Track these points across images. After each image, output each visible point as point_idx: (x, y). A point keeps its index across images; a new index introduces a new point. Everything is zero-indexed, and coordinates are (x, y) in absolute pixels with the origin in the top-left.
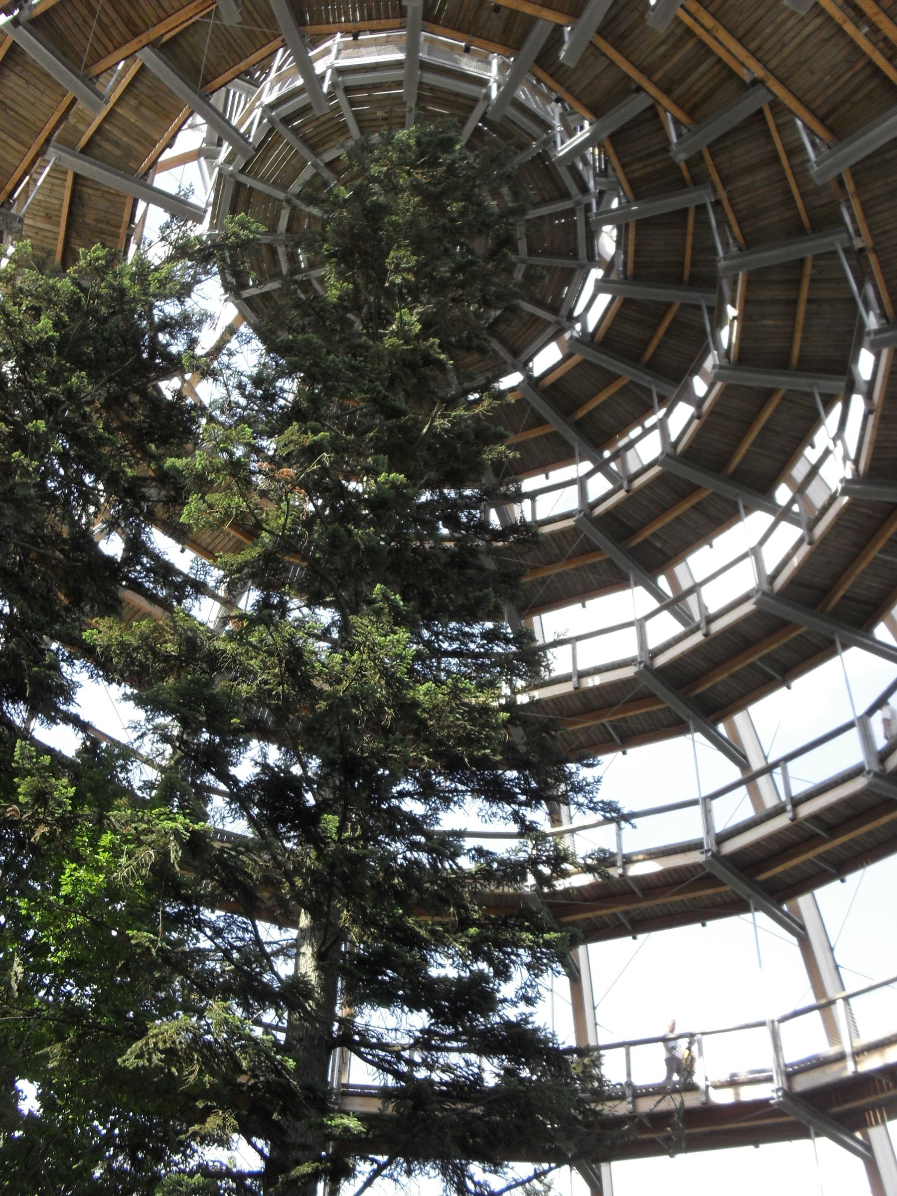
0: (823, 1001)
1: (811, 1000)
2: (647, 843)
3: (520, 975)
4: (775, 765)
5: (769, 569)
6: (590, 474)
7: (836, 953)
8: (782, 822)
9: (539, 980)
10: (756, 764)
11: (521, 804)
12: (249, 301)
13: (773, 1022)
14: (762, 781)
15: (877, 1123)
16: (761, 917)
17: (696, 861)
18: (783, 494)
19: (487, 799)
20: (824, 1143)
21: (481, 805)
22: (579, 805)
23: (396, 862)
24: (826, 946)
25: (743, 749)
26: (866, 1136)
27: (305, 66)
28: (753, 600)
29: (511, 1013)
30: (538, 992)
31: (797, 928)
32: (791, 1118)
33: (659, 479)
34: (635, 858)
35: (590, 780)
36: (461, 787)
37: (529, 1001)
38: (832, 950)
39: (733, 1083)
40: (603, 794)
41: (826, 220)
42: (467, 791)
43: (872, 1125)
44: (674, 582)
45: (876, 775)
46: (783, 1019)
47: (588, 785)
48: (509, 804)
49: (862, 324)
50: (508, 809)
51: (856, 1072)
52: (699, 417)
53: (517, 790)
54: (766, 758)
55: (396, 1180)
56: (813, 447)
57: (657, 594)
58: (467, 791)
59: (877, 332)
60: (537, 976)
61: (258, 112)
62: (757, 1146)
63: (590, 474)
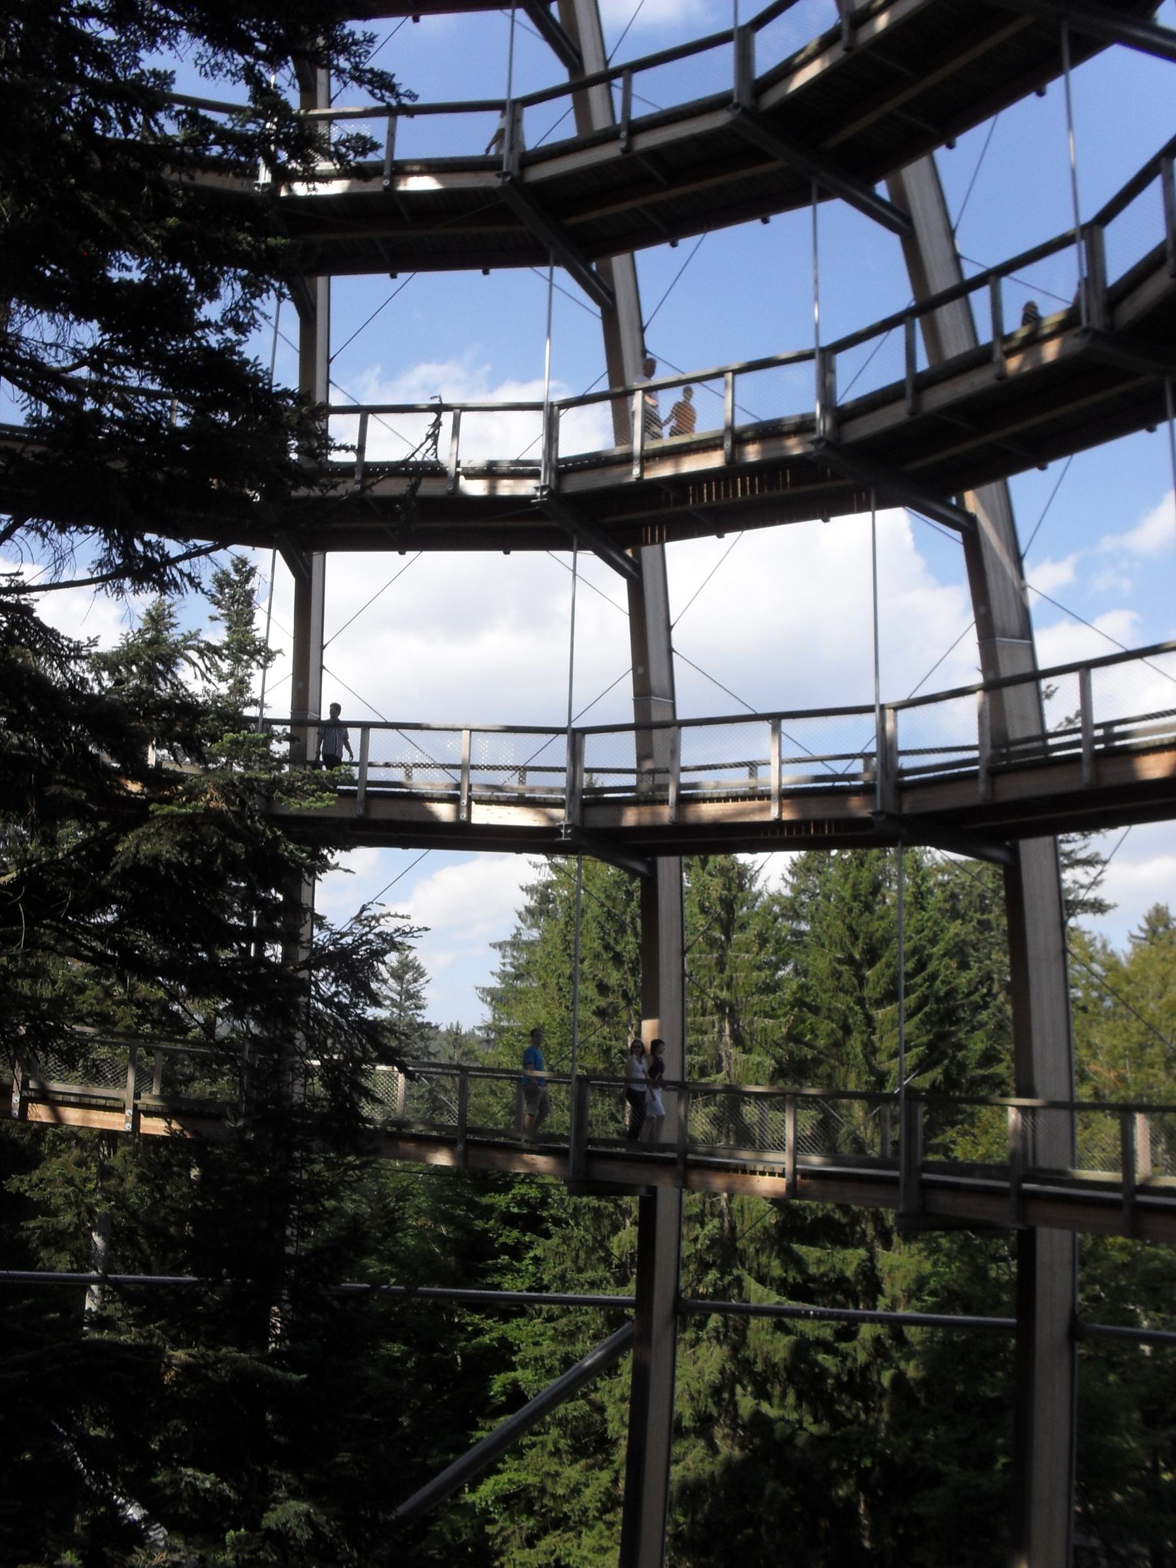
0: (619, 390)
1: (604, 386)
2: (429, 149)
3: (230, 292)
4: (617, 73)
5: (1115, 272)
7: (647, 335)
8: (611, 151)
9: (257, 302)
10: (592, 67)
11: (259, 56)
13: (552, 405)
15: (653, 542)
17: (489, 185)
19: (211, 41)
20: (589, 560)
21: (201, 49)
22: (340, 72)
23: (70, 107)
24: (636, 324)
25: (579, 45)
26: (638, 555)
29: (213, 340)
30: (253, 317)
31: (603, 293)
32: (554, 524)
34: (408, 168)
35: (359, 36)
36: (173, 16)
37: (241, 328)
38: (642, 330)
39: (491, 472)
40: (376, 62)
42: (181, 24)
43: (647, 544)
45: (745, 111)
46: (567, 404)
47: (355, 43)
48: (242, 54)
50: (240, 60)
51: (640, 479)
53: (255, 34)
54: (607, 63)
55: (44, 535)
58: (181, 24)
60: (254, 296)
62: (507, 553)
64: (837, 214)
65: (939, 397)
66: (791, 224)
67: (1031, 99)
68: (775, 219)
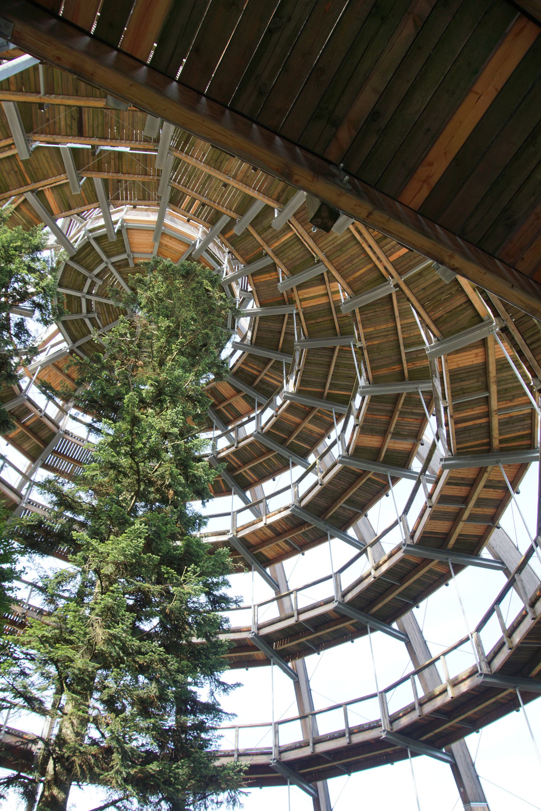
6: (220, 436)
8: (291, 622)
12: (64, 323)
14: (286, 599)
16: (276, 668)
18: (312, 459)
20: (295, 789)
27: (107, 216)
28: (290, 509)
31: (294, 675)
33: (251, 444)
41: (347, 333)
44: (254, 495)
46: (479, 629)
49: (358, 383)
52: (276, 416)
56: (329, 438)
57: (245, 499)
59: (363, 387)
61: (82, 233)
63: (220, 436)
64: (378, 638)
65: (428, 708)
66: (361, 641)
67: (349, 643)
68: (356, 641)
